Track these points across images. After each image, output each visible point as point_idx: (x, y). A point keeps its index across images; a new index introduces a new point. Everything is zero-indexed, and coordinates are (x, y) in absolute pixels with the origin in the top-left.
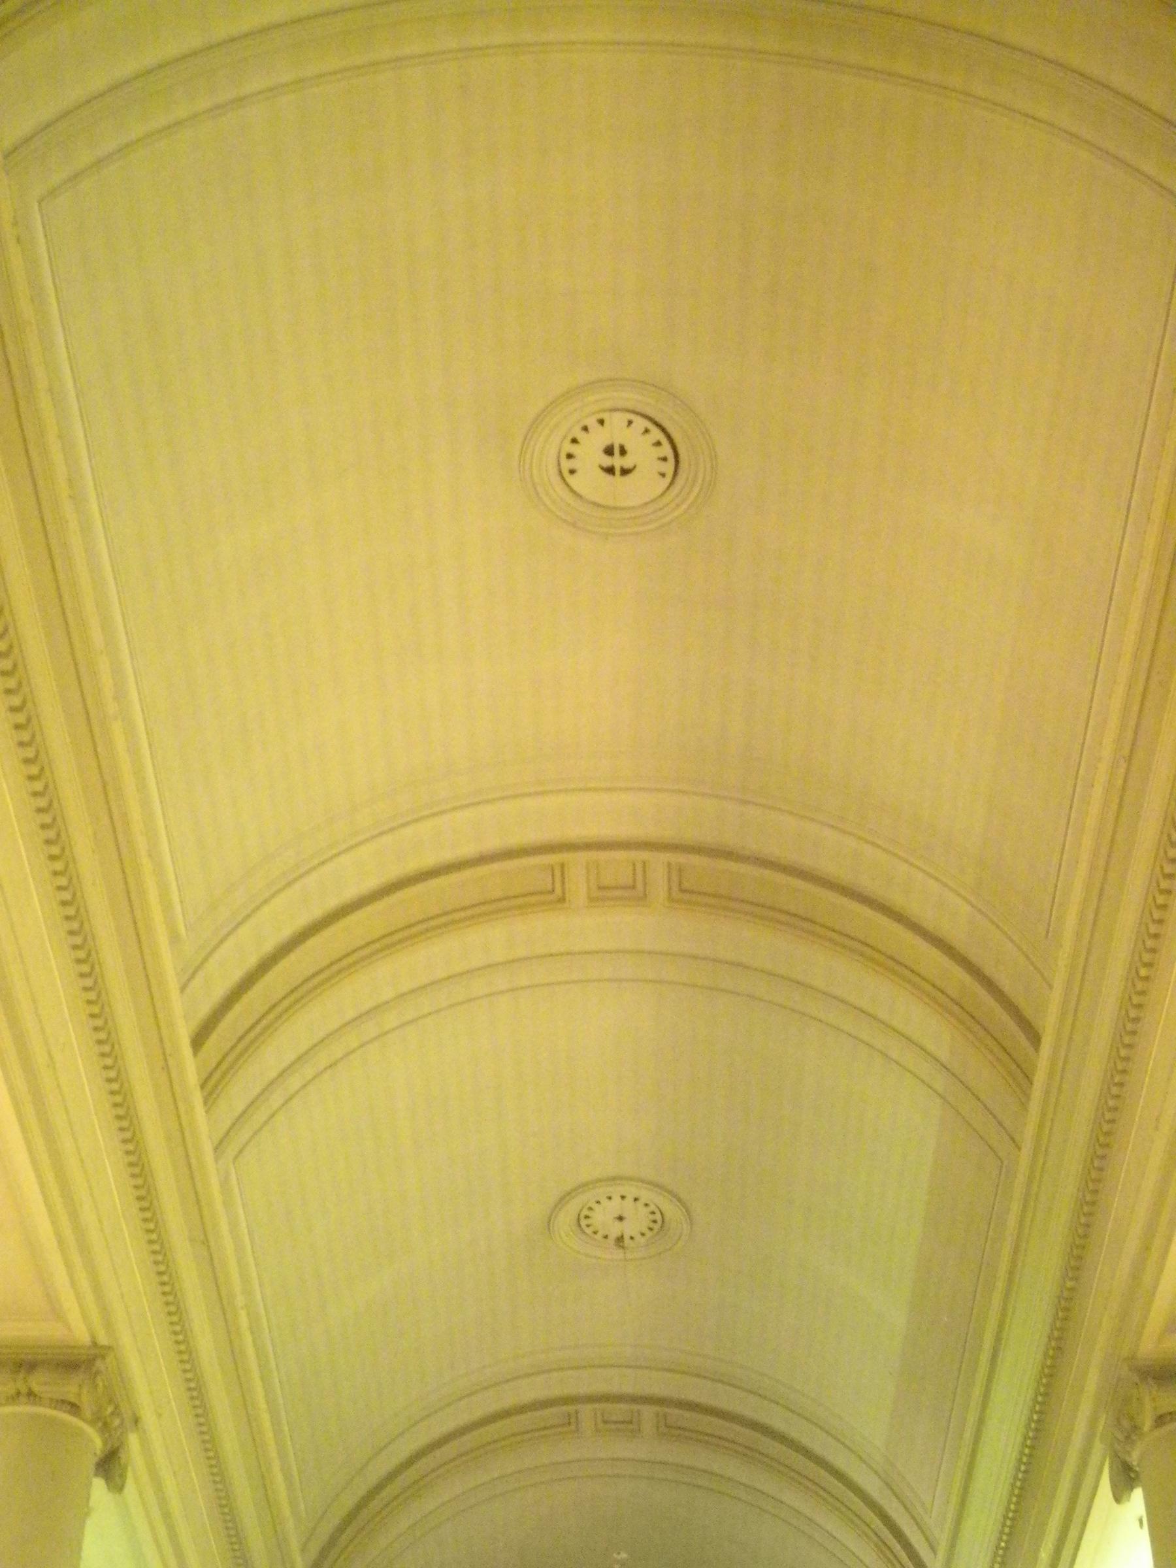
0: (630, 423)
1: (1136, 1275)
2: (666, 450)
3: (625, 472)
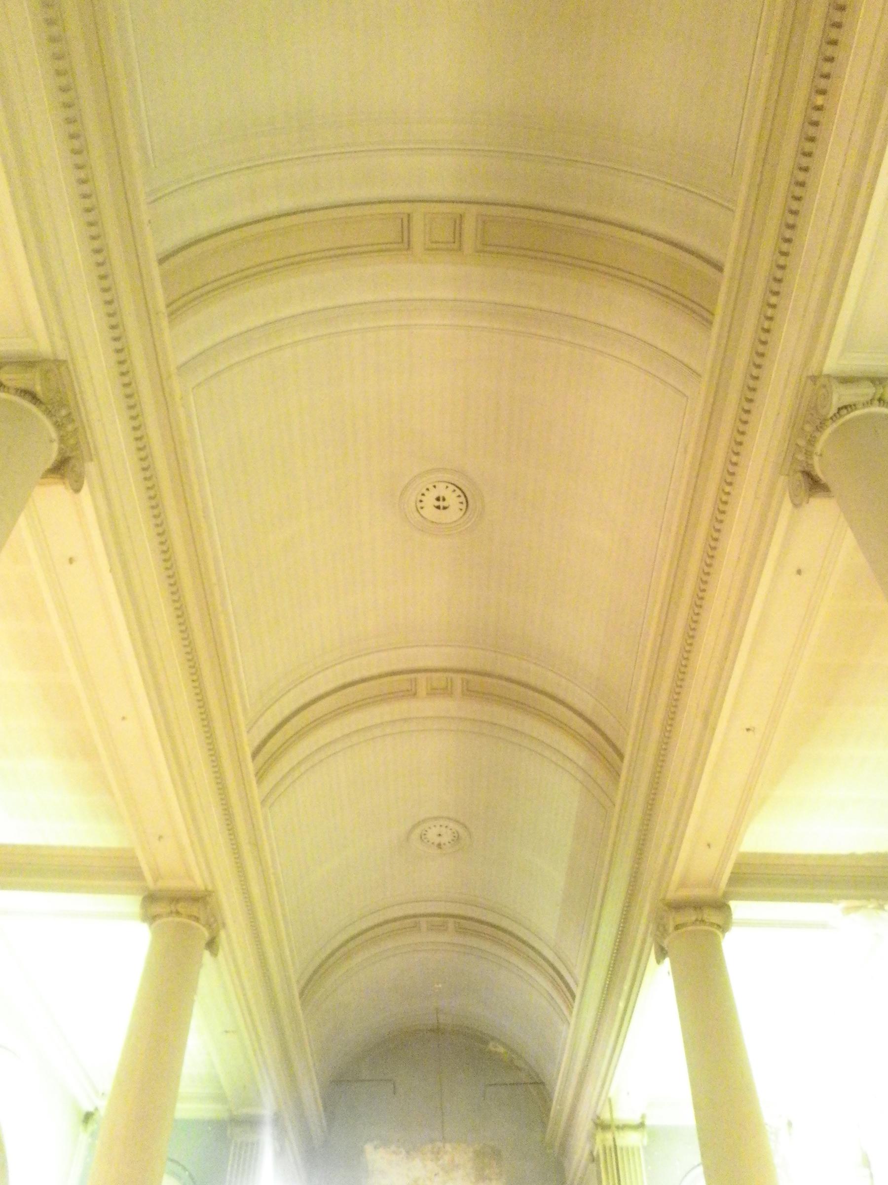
0: (447, 487)
1: (666, 862)
2: (463, 499)
3: (445, 508)
